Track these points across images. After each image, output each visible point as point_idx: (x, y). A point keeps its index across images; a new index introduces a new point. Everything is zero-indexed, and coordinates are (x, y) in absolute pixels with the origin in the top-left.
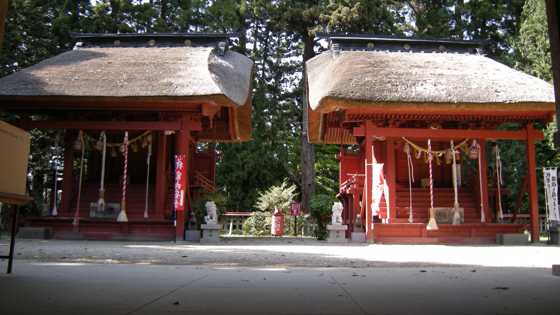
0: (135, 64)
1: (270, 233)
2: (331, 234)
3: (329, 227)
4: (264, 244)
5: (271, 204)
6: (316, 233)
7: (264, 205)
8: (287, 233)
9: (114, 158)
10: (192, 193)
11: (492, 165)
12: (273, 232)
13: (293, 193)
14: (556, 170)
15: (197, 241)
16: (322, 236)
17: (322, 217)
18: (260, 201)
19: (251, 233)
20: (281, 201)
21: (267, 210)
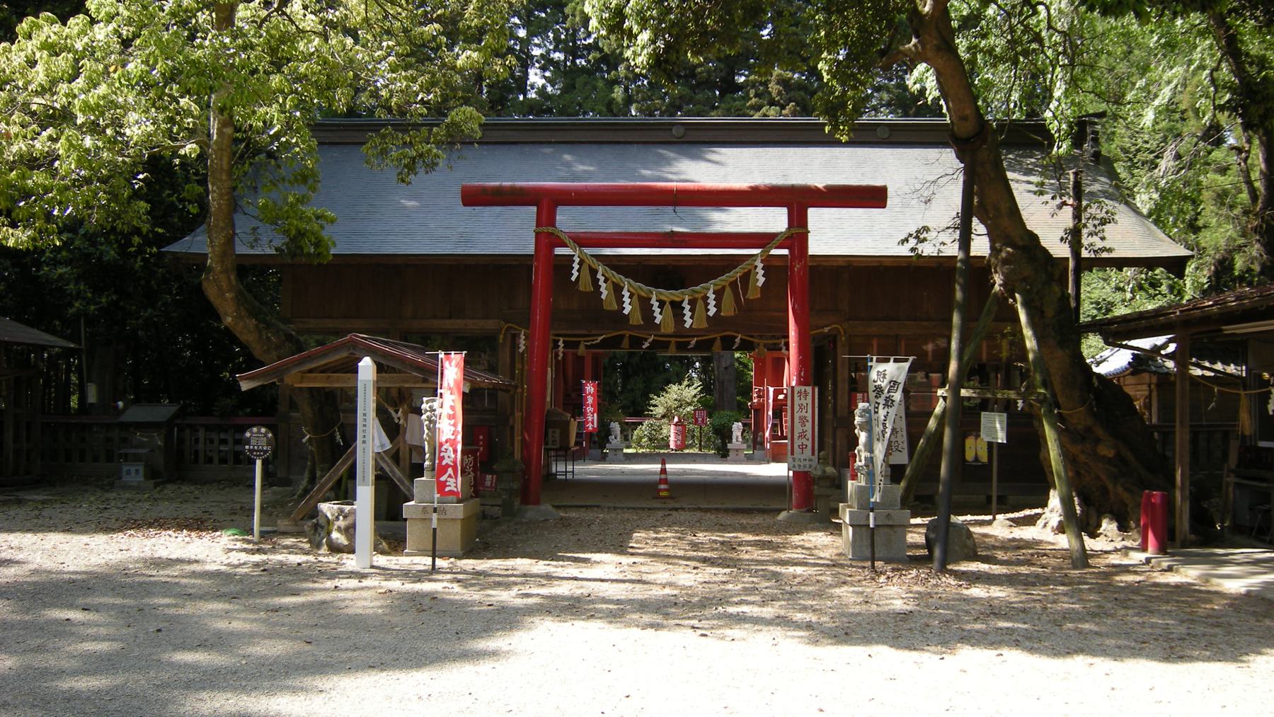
0: (615, 508)
1: (668, 446)
2: (731, 453)
3: (729, 446)
4: (694, 462)
5: (669, 409)
6: (718, 449)
7: (660, 411)
8: (691, 446)
9: (594, 378)
10: (601, 410)
11: (868, 455)
12: (672, 445)
13: (337, 34)
14: (906, 365)
15: (603, 459)
16: (723, 454)
17: (724, 434)
18: (655, 406)
19: (642, 447)
20: (681, 403)
21: (663, 417)
